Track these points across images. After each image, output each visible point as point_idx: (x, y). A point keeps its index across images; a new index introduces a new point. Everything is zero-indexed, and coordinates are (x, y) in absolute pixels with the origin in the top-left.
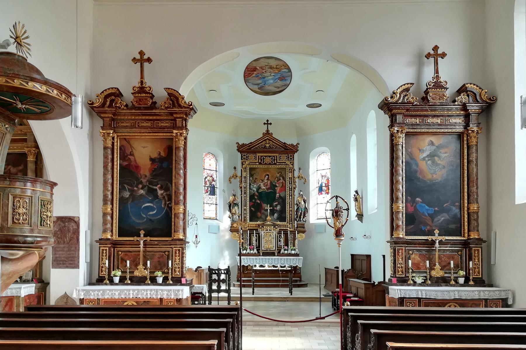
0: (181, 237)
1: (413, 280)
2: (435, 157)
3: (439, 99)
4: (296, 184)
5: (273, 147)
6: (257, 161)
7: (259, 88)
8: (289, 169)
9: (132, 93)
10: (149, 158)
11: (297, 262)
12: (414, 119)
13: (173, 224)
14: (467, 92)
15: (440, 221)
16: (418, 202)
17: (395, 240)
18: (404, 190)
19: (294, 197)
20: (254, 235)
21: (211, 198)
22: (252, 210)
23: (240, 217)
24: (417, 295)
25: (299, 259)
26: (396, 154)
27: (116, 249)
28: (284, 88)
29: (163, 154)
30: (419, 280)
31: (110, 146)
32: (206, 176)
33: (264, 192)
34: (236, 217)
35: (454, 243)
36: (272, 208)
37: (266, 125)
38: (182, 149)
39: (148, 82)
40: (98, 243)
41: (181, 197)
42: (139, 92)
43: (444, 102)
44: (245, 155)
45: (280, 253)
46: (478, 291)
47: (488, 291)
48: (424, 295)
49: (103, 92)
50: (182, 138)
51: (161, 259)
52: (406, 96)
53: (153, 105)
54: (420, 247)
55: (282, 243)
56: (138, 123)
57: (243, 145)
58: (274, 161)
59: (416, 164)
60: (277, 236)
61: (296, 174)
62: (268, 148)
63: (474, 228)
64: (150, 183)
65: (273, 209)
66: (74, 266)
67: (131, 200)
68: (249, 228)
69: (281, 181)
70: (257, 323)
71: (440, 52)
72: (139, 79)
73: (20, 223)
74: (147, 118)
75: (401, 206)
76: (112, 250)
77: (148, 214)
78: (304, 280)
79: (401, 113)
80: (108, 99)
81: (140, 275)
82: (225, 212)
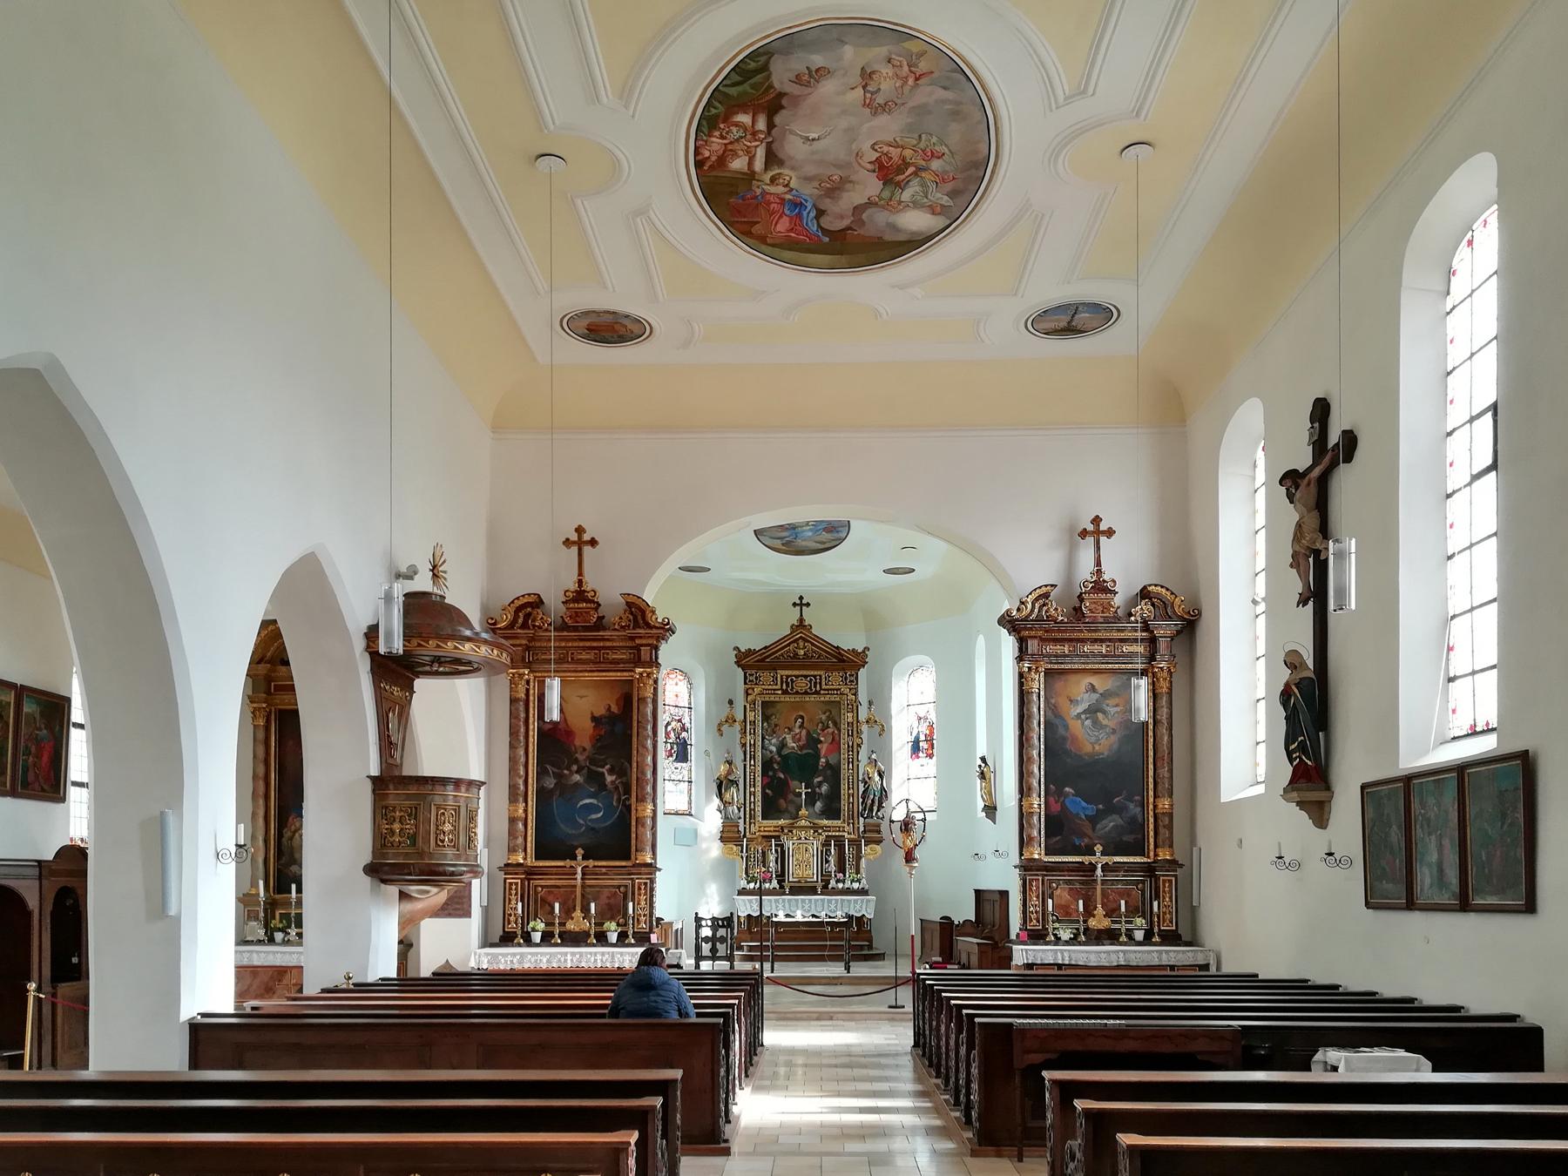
0: (649, 861)
1: (1055, 935)
2: (1098, 714)
3: (1103, 612)
5: (812, 656)
6: (779, 687)
7: (783, 544)
8: (848, 705)
9: (563, 602)
10: (590, 716)
11: (864, 907)
13: (633, 836)
14: (1151, 599)
16: (1068, 794)
17: (1025, 863)
18: (1042, 773)
19: (858, 765)
20: (771, 850)
22: (767, 794)
23: (742, 809)
24: (1055, 959)
25: (868, 901)
26: (1028, 710)
27: (532, 882)
29: (614, 709)
30: (1066, 935)
32: (668, 719)
34: (733, 809)
35: (1130, 868)
36: (810, 790)
37: (798, 608)
38: (650, 700)
39: (591, 583)
40: (503, 873)
41: (649, 789)
42: (574, 600)
43: (1110, 617)
46: (1157, 951)
47: (1174, 951)
48: (1067, 958)
49: (513, 602)
50: (651, 682)
51: (612, 901)
52: (1044, 605)
54: (1069, 876)
55: (832, 867)
56: (572, 654)
57: (750, 652)
58: (815, 687)
60: (822, 851)
61: (863, 715)
63: (1163, 842)
64: (592, 761)
65: (814, 791)
67: (558, 793)
68: (762, 834)
69: (830, 730)
70: (782, 1015)
71: (1103, 527)
72: (575, 578)
73: (444, 846)
74: (588, 644)
75: (1037, 802)
76: (526, 883)
77: (589, 818)
78: (879, 945)
79: (1036, 637)
80: (520, 614)
81: (577, 929)
82: (708, 800)
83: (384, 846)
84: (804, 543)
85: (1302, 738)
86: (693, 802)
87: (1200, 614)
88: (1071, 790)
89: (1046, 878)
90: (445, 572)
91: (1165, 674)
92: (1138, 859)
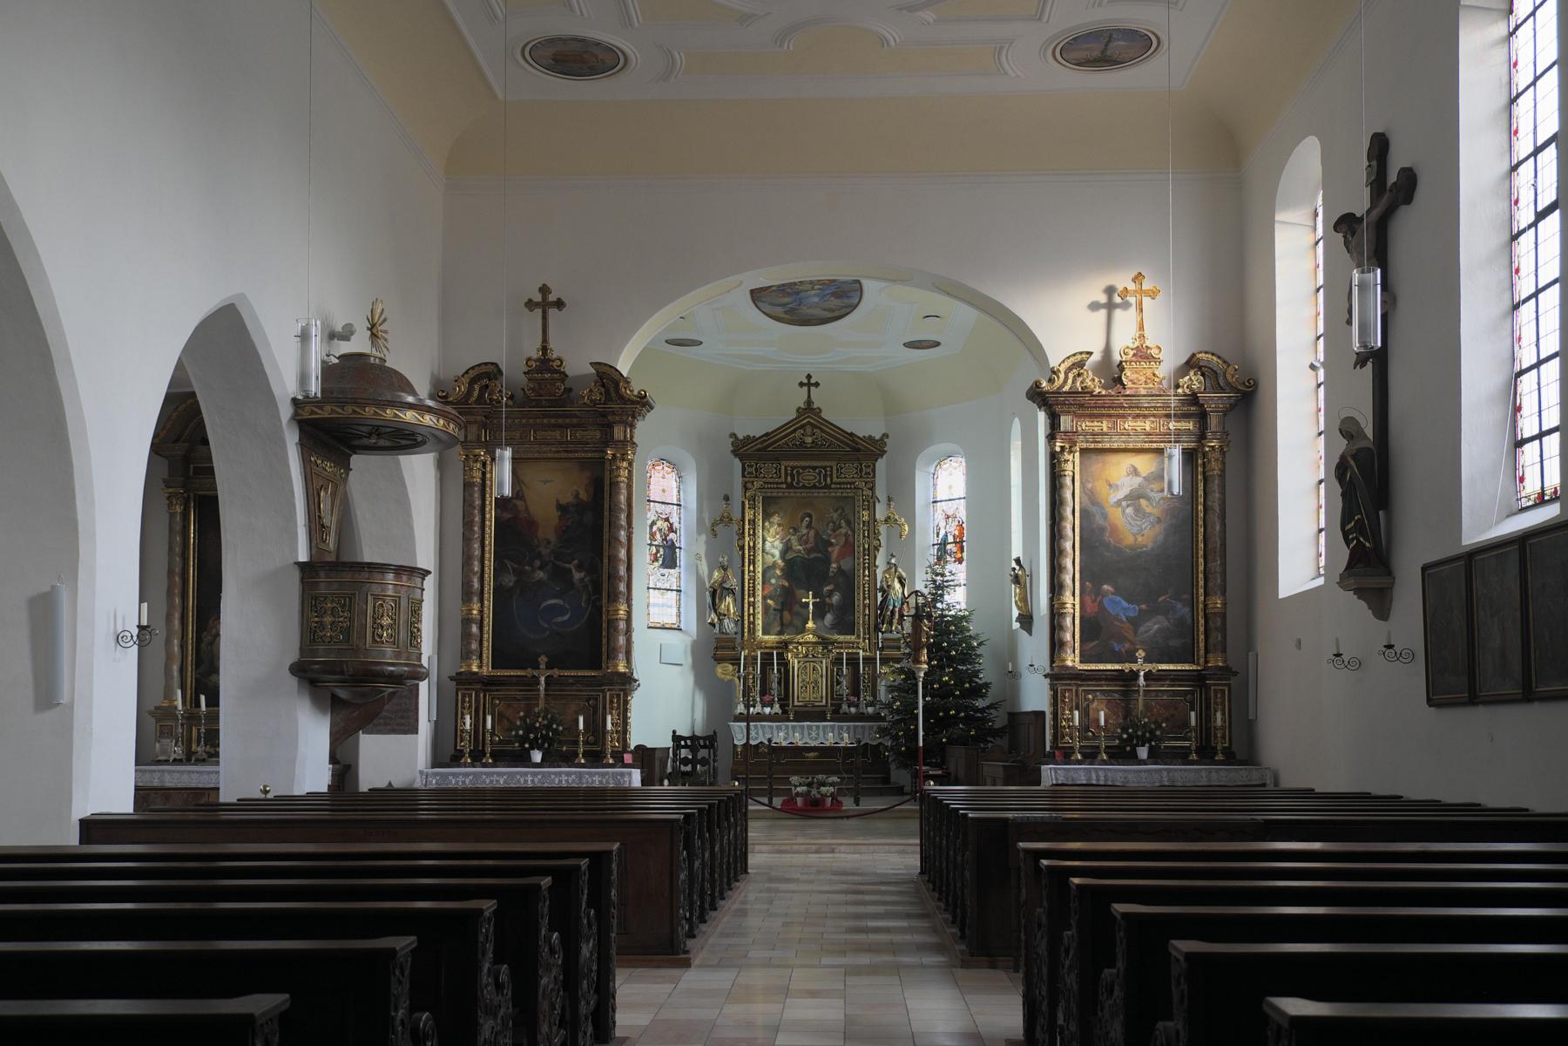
2: (1141, 500)
4: (880, 538)
7: (785, 312)
8: (864, 501)
9: (525, 373)
10: (555, 503)
12: (1098, 422)
15: (1151, 632)
18: (1077, 568)
20: (773, 669)
21: (667, 575)
28: (844, 311)
29: (583, 496)
31: (478, 480)
33: (799, 559)
36: (818, 600)
37: (806, 388)
39: (556, 350)
42: (538, 371)
44: (752, 466)
45: (839, 713)
47: (1225, 770)
48: (1102, 778)
49: (467, 372)
52: (1079, 375)
53: (565, 396)
54: (1108, 685)
55: (844, 688)
57: (749, 440)
58: (825, 480)
59: (1102, 514)
60: (832, 671)
61: (881, 512)
62: (809, 446)
66: (407, 728)
69: (843, 531)
72: (539, 343)
76: (482, 695)
77: (554, 621)
83: (313, 641)
84: (810, 311)
85: (1359, 516)
86: (682, 615)
87: (1256, 385)
88: (1110, 588)
89: (1081, 689)
90: (386, 332)
91: (1217, 454)
92: (1187, 667)
